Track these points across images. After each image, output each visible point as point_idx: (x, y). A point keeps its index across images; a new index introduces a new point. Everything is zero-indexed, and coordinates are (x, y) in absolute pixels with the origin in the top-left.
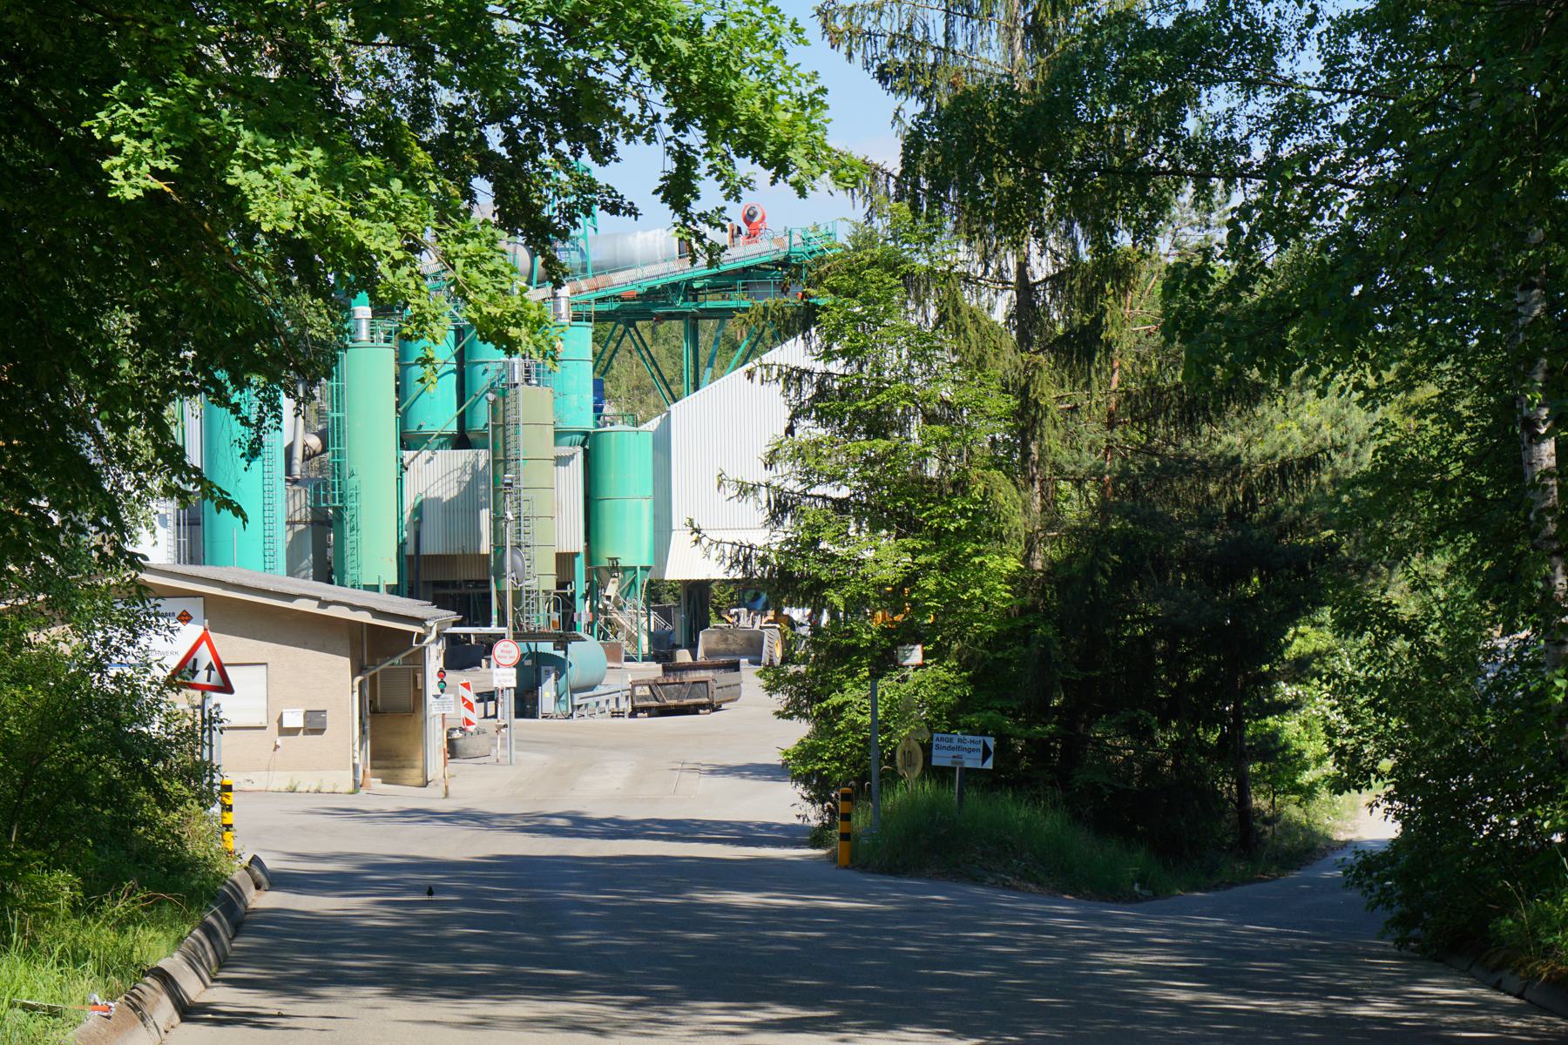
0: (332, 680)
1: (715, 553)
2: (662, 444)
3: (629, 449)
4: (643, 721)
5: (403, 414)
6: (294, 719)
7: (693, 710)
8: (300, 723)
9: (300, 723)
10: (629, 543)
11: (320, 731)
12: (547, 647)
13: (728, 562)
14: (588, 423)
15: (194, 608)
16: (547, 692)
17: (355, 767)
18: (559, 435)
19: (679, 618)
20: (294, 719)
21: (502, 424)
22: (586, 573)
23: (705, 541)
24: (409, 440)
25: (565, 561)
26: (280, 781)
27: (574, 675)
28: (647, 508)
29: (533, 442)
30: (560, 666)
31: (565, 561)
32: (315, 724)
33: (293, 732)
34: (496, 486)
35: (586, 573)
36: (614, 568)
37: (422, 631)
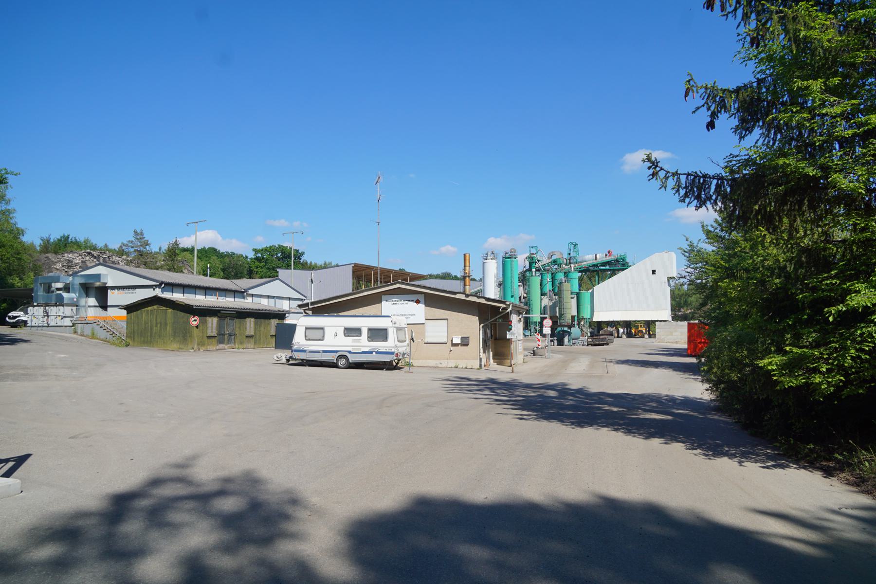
0: (472, 326)
1: (671, 182)
2: (592, 295)
3: (586, 295)
4: (590, 347)
5: (541, 290)
6: (457, 340)
7: (603, 345)
8: (459, 342)
9: (459, 342)
10: (586, 314)
11: (467, 345)
12: (566, 329)
13: (682, 192)
14: (577, 291)
15: (421, 298)
16: (566, 339)
17: (481, 359)
18: (572, 293)
19: (596, 329)
20: (457, 340)
21: (560, 290)
22: (578, 319)
23: (662, 174)
24: (543, 294)
25: (573, 317)
26: (452, 364)
27: (573, 335)
28: (589, 307)
29: (566, 294)
30: (569, 333)
31: (573, 317)
32: (465, 342)
33: (457, 345)
34: (560, 303)
35: (578, 319)
36: (583, 319)
37: (503, 306)
